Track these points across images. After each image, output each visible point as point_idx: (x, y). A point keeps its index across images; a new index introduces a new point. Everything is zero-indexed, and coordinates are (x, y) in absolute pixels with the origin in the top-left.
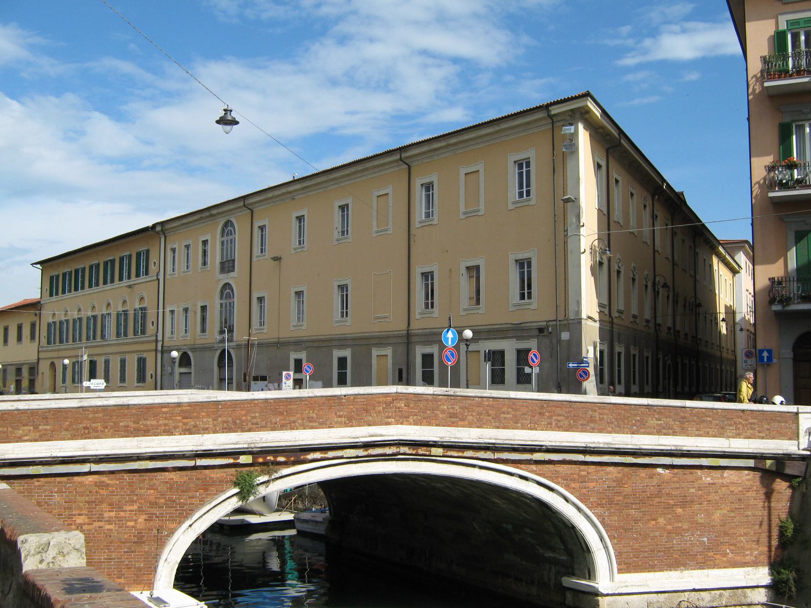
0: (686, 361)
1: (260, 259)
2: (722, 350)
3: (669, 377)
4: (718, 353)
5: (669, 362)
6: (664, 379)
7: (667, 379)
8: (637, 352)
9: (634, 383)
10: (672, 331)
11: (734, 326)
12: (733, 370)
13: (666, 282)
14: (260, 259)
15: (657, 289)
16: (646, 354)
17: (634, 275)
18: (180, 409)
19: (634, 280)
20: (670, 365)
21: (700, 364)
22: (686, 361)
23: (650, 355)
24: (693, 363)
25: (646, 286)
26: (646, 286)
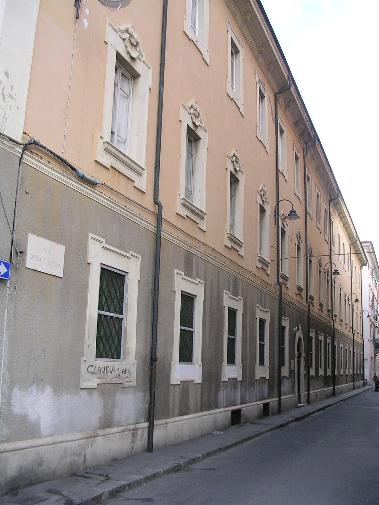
0: (321, 338)
1: (359, 356)
2: (354, 332)
3: (299, 356)
4: (351, 335)
5: (299, 334)
6: (292, 357)
7: (296, 359)
8: (239, 306)
9: (262, 363)
10: (304, 294)
11: (362, 312)
12: (362, 353)
13: (369, 314)
14: (359, 356)
15: (281, 225)
16: (259, 315)
17: (299, 243)
18: (86, 432)
19: (234, 180)
20: (300, 339)
21: (336, 343)
22: (321, 338)
23: (267, 317)
24: (329, 341)
25: (262, 211)
26: (262, 211)
